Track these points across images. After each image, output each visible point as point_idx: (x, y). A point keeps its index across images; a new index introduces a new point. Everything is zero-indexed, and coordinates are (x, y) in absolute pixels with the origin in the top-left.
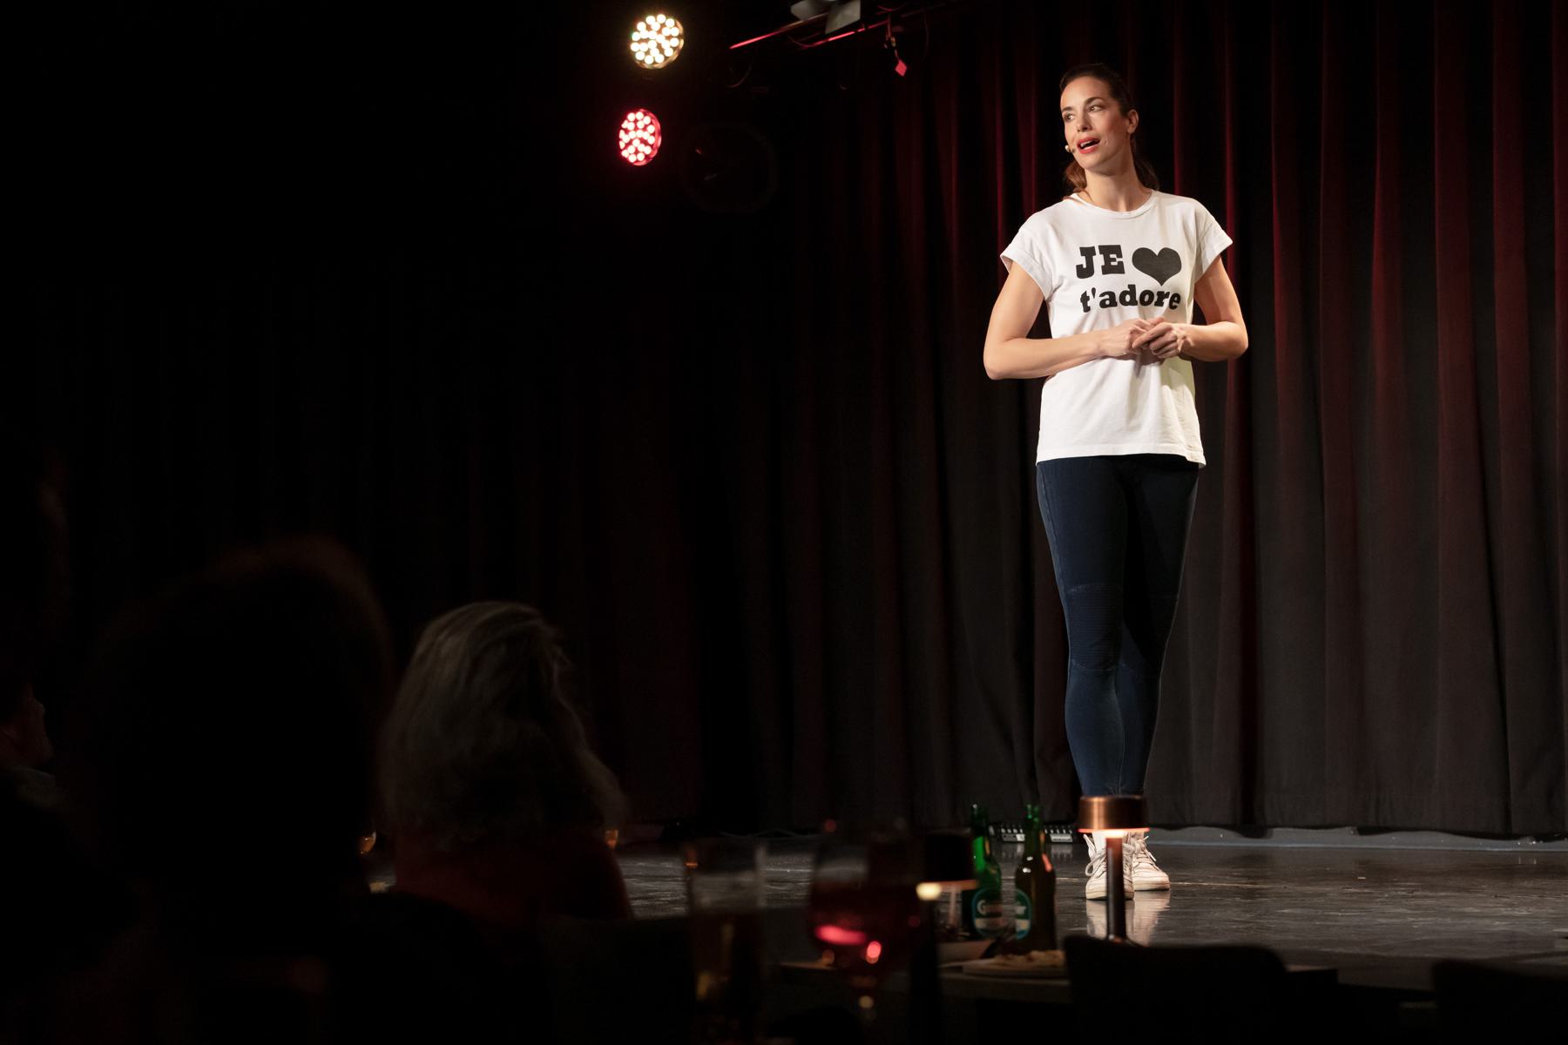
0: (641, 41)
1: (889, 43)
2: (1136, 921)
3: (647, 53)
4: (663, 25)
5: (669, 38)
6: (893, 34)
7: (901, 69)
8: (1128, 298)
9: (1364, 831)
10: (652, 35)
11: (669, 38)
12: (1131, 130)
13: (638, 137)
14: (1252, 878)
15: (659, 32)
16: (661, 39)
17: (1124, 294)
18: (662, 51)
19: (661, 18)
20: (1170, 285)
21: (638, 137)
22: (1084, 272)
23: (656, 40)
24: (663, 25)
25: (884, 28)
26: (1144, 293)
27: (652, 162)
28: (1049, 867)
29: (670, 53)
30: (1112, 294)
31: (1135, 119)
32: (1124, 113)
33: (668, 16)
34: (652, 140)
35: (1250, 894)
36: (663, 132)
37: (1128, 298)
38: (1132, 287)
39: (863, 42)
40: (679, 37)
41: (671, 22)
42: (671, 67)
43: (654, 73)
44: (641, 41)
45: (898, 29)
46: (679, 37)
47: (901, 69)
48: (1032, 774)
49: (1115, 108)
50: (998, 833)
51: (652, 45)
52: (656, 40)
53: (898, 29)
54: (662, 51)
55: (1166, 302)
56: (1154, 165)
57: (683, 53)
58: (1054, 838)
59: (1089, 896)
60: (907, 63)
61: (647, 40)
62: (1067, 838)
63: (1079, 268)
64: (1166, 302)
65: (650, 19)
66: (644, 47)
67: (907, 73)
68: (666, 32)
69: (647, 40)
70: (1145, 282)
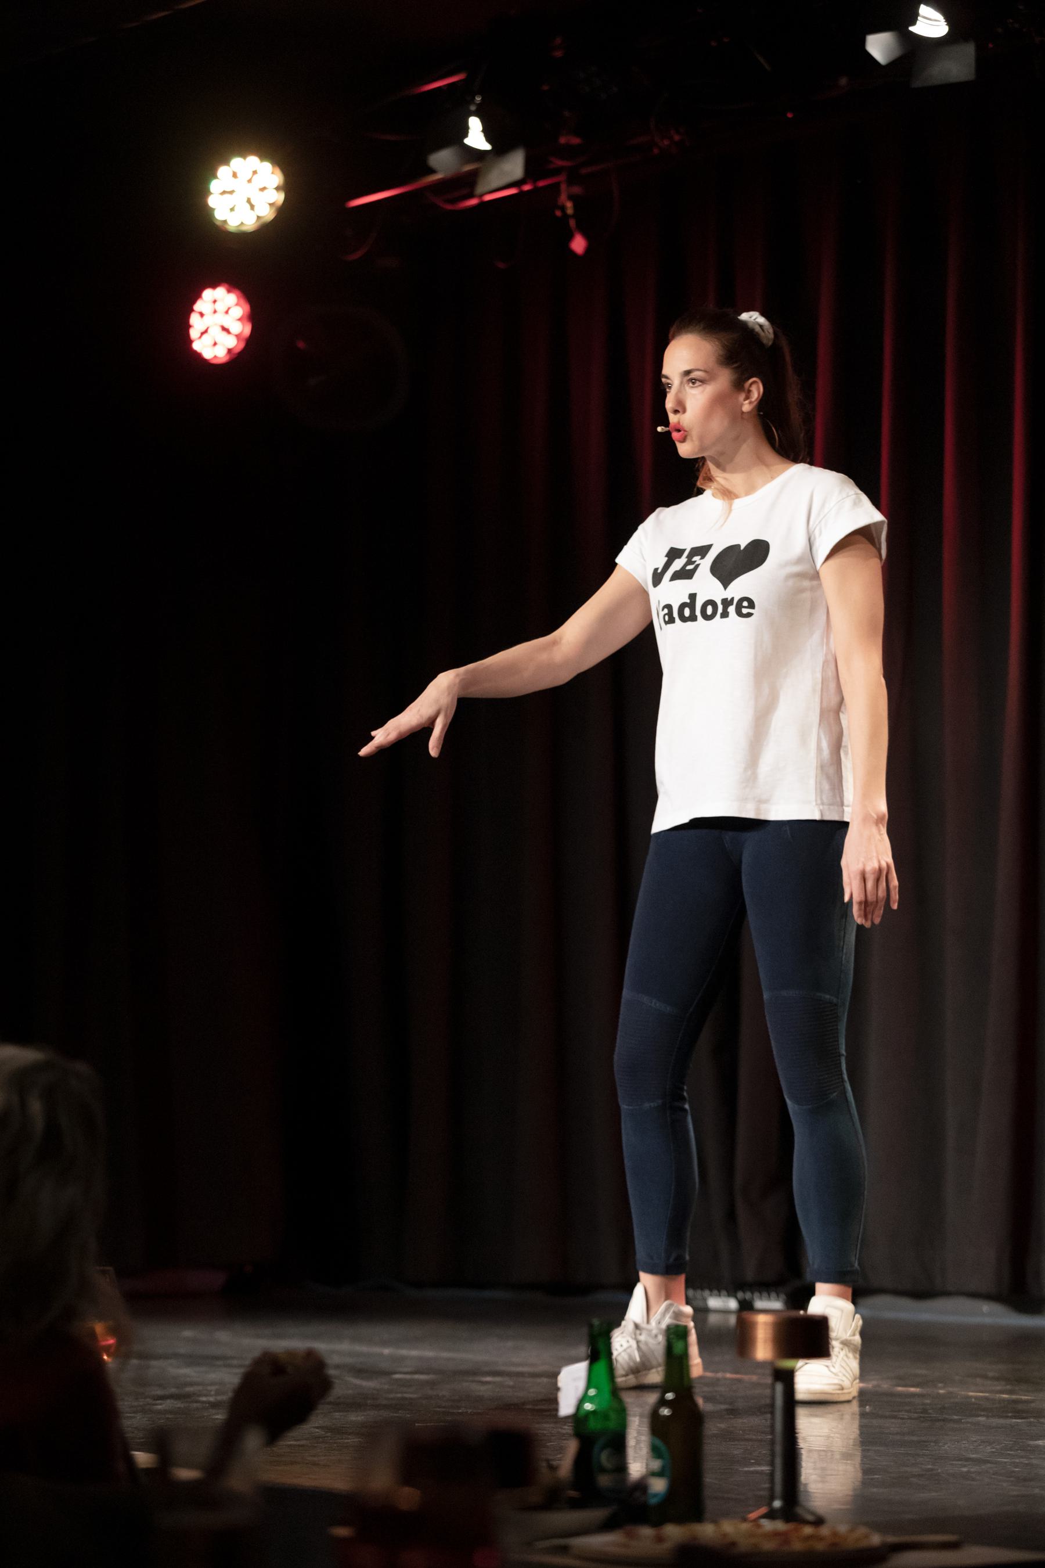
1: (563, 208)
6: (571, 198)
7: (579, 245)
8: (687, 612)
12: (747, 407)
13: (218, 324)
14: (1018, 1380)
17: (682, 607)
20: (742, 586)
21: (218, 324)
22: (657, 578)
23: (245, 192)
25: (556, 187)
27: (237, 360)
29: (237, 328)
30: (669, 607)
31: (757, 390)
32: (739, 385)
35: (1016, 1410)
36: (254, 317)
37: (687, 612)
38: (693, 597)
39: (521, 210)
42: (265, 230)
43: (242, 238)
45: (576, 190)
47: (579, 245)
48: (731, 1216)
49: (724, 378)
51: (216, 333)
52: (245, 192)
53: (576, 190)
55: (732, 609)
56: (788, 435)
57: (283, 212)
60: (586, 236)
62: (733, 1304)
63: (656, 570)
64: (732, 609)
65: (198, 306)
67: (588, 250)
70: (706, 586)
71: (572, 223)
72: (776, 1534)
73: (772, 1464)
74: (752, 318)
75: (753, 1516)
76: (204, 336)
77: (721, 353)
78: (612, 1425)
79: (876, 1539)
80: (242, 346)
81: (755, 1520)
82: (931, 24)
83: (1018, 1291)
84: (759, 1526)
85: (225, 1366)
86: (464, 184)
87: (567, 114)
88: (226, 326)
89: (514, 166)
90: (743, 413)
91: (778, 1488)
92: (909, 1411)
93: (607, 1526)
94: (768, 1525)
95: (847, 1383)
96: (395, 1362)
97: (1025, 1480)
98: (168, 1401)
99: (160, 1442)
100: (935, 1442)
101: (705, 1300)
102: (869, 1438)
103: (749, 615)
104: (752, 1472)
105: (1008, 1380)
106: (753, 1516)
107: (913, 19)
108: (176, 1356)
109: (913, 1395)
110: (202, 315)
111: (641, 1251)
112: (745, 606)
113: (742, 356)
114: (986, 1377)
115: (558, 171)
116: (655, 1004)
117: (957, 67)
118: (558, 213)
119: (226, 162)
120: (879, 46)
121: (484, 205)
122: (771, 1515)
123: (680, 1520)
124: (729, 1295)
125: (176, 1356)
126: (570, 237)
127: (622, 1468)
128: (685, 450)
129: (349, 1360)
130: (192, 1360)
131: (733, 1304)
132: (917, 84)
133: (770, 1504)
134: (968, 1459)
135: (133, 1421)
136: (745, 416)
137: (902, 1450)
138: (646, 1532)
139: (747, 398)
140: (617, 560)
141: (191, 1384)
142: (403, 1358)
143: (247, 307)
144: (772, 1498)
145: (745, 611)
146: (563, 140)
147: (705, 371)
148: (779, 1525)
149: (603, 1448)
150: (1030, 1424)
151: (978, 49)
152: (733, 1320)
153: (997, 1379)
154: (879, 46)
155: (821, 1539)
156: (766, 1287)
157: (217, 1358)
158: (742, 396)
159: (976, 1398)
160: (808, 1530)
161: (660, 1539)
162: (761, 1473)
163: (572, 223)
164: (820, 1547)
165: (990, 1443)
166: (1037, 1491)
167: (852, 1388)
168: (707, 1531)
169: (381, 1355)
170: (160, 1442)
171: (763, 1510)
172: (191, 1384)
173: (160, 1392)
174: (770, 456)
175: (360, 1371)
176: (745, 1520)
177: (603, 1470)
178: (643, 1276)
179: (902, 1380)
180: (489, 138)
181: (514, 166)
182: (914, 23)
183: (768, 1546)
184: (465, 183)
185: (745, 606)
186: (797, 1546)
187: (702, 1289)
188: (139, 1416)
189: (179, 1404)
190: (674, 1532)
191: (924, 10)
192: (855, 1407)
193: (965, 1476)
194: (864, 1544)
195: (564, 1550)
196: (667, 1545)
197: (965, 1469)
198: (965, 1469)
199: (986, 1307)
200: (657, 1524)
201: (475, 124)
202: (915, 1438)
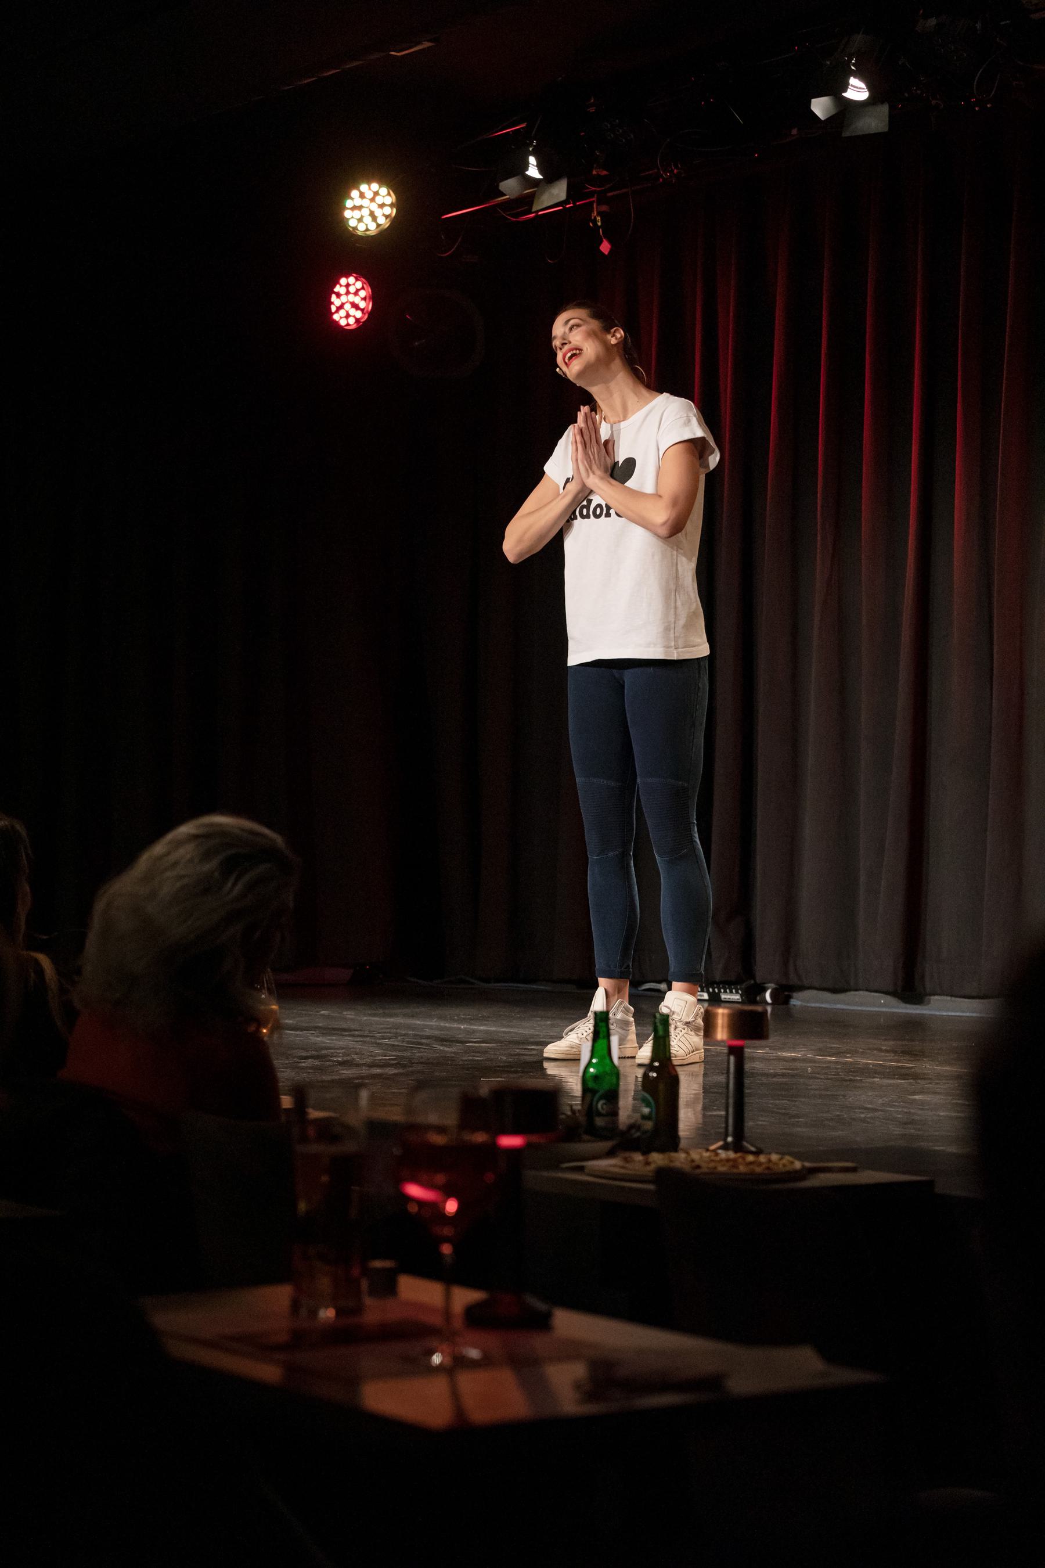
0: (354, 208)
1: (595, 221)
3: (360, 220)
4: (376, 194)
7: (605, 247)
13: (350, 302)
14: (908, 1053)
15: (372, 200)
18: (374, 218)
19: (375, 186)
21: (350, 302)
23: (369, 207)
24: (376, 194)
33: (381, 183)
34: (362, 305)
40: (392, 205)
41: (384, 191)
42: (383, 235)
44: (354, 208)
45: (604, 208)
46: (392, 205)
47: (605, 247)
51: (365, 212)
52: (369, 207)
53: (604, 208)
54: (374, 218)
60: (610, 242)
61: (360, 208)
66: (357, 214)
68: (379, 200)
72: (728, 1160)
73: (727, 1111)
75: (712, 1147)
79: (798, 1165)
81: (714, 1151)
82: (857, 91)
83: (909, 989)
84: (717, 1154)
85: (350, 1036)
86: (525, 202)
89: (559, 191)
91: (731, 1129)
92: (826, 1074)
93: (610, 1154)
94: (723, 1154)
96: (471, 1031)
97: (906, 1123)
98: (310, 1060)
99: (300, 1093)
100: (844, 1096)
104: (715, 1116)
105: (895, 1052)
106: (712, 1147)
107: (845, 87)
108: (316, 1028)
109: (830, 1062)
110: (362, 196)
111: (599, 963)
114: (881, 1050)
115: (591, 194)
117: (875, 122)
120: (820, 107)
121: (538, 217)
122: (726, 1147)
123: (661, 1150)
124: (702, 991)
125: (316, 1028)
127: (614, 1113)
129: (437, 1033)
130: (327, 1031)
132: (846, 134)
133: (725, 1140)
134: (866, 1108)
135: (285, 1075)
137: (820, 1101)
138: (638, 1157)
140: (546, 468)
141: (326, 1048)
142: (474, 1031)
144: (727, 1136)
148: (731, 1155)
149: (600, 1098)
150: (910, 1084)
151: (890, 108)
153: (886, 1051)
154: (820, 107)
155: (760, 1164)
156: (729, 984)
157: (344, 1030)
159: (873, 1065)
160: (751, 1158)
161: (648, 1163)
162: (721, 1116)
164: (758, 1170)
165: (881, 1097)
166: (913, 1131)
168: (679, 1159)
169: (460, 1029)
170: (300, 1093)
171: (721, 1143)
172: (326, 1048)
173: (304, 1054)
174: (644, 392)
175: (443, 1040)
176: (707, 1150)
177: (599, 1114)
178: (602, 981)
179: (822, 1052)
180: (541, 173)
181: (559, 191)
182: (845, 91)
183: (722, 1169)
184: (525, 202)
186: (742, 1169)
188: (288, 1070)
189: (317, 1063)
190: (658, 1159)
191: (853, 81)
193: (864, 1120)
194: (789, 1168)
195: (581, 1169)
196: (653, 1167)
197: (863, 1116)
198: (863, 1116)
199: (883, 999)
200: (646, 1152)
201: (532, 160)
202: (828, 1093)
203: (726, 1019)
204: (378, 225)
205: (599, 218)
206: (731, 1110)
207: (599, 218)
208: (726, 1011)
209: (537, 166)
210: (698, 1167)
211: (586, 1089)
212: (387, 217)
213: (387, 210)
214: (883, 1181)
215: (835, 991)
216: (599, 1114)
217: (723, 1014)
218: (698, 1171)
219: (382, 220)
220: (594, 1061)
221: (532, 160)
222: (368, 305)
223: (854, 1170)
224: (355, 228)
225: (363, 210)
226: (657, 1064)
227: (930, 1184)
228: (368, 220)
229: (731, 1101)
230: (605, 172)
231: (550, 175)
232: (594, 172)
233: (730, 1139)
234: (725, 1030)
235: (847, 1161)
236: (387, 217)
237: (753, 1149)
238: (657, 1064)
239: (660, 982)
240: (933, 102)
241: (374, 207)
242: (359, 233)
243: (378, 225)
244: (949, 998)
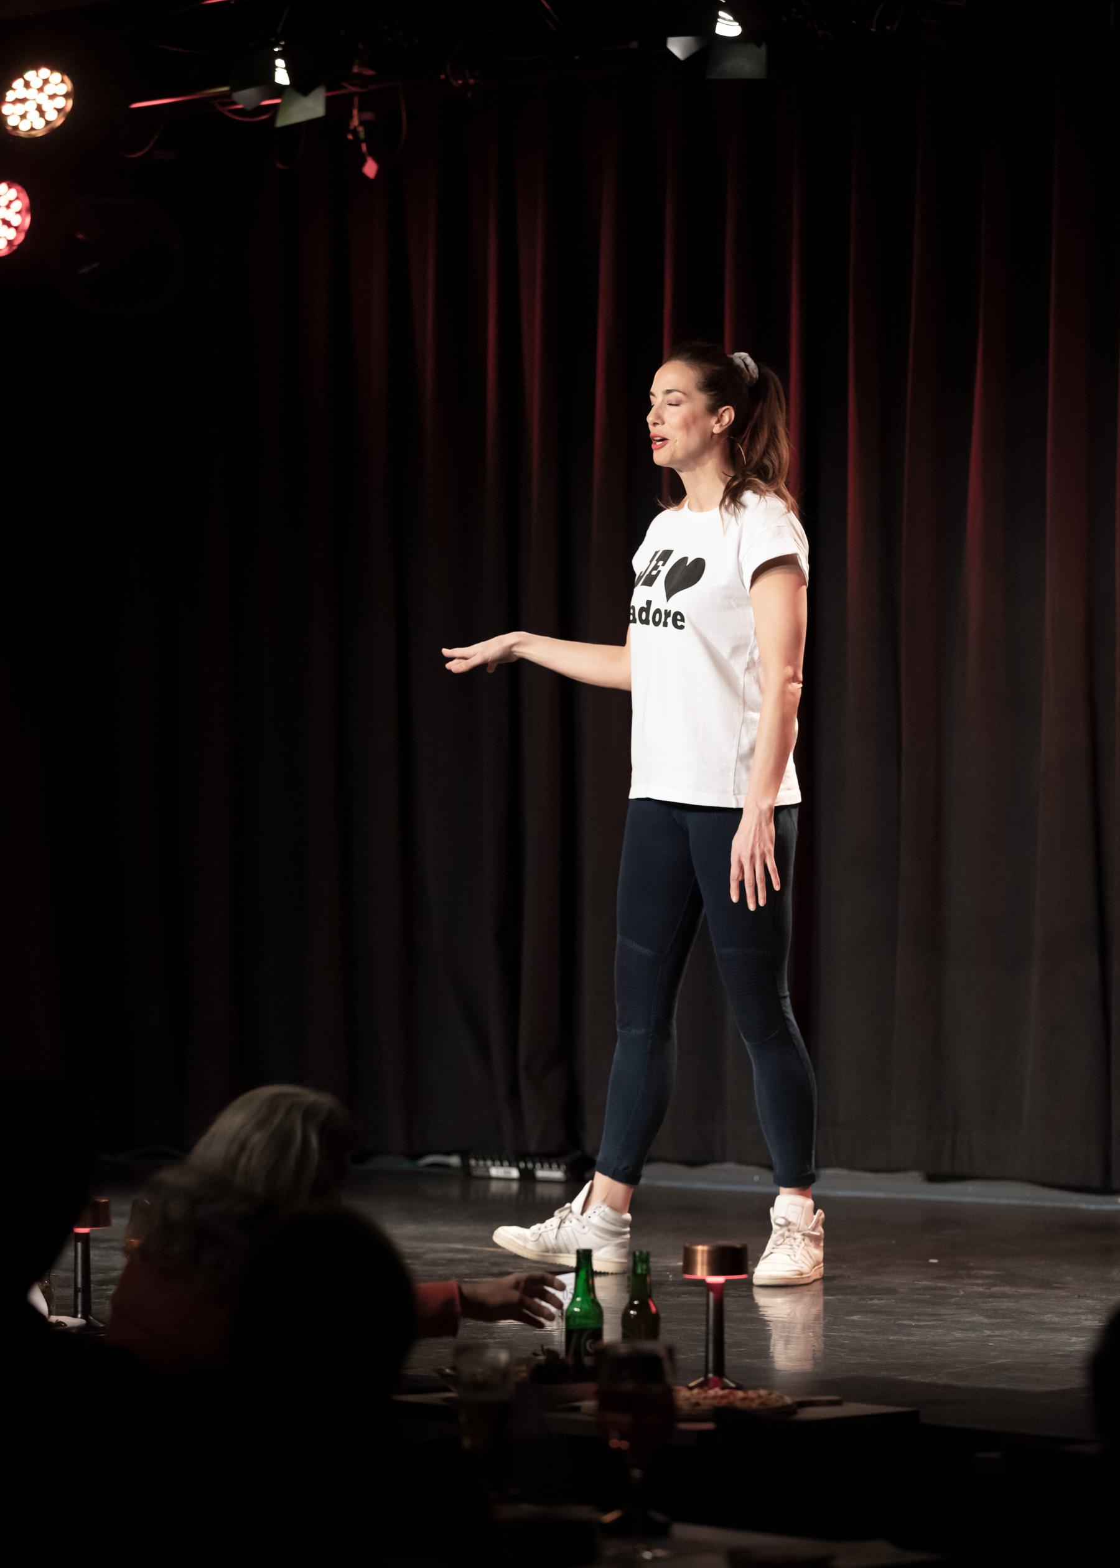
0: (17, 101)
2: (791, 1364)
3: (23, 117)
4: (46, 81)
5: (52, 97)
7: (370, 169)
9: (934, 1177)
10: (31, 93)
11: (52, 97)
12: (717, 429)
15: (41, 90)
16: (42, 99)
18: (41, 112)
19: (45, 72)
20: (682, 601)
24: (46, 81)
26: (658, 611)
28: (653, 1309)
31: (728, 415)
33: (53, 68)
34: (16, 220)
36: (34, 209)
38: (649, 603)
40: (66, 96)
41: (56, 77)
42: (54, 135)
44: (17, 101)
45: (369, 116)
46: (66, 96)
47: (370, 169)
48: (514, 1091)
49: (701, 400)
50: (465, 1165)
51: (30, 107)
54: (41, 112)
55: (670, 620)
58: (541, 1174)
59: (756, 1281)
60: (377, 160)
61: (23, 101)
62: (514, 1173)
65: (30, 75)
66: (20, 109)
67: (379, 173)
68: (49, 89)
69: (23, 101)
71: (364, 147)
74: (743, 358)
76: (19, 105)
77: (702, 380)
78: (591, 1323)
80: (22, 237)
87: (361, 46)
88: (44, 108)
90: (713, 434)
91: (711, 1365)
95: (806, 1268)
101: (487, 1169)
102: (831, 1316)
103: (682, 627)
110: (27, 85)
112: (677, 619)
113: (720, 387)
116: (646, 951)
117: (747, 66)
118: (350, 137)
119: (20, 75)
124: (510, 1166)
126: (363, 162)
128: (660, 457)
131: (514, 1173)
132: (712, 76)
136: (715, 437)
139: (718, 421)
143: (27, 200)
144: (707, 1372)
145: (679, 623)
146: (356, 70)
147: (684, 393)
149: (587, 1339)
152: (515, 1186)
156: (548, 1158)
158: (714, 420)
163: (364, 147)
166: (869, 1360)
167: (819, 1272)
177: (588, 1354)
185: (677, 619)
187: (485, 1159)
191: (721, 13)
192: (819, 1286)
201: (280, 63)
203: (705, 1255)
204: (48, 123)
205: (361, 129)
206: (711, 1346)
207: (361, 129)
208: (705, 1248)
209: (286, 68)
210: (698, 1404)
211: (569, 1333)
212: (59, 111)
213: (61, 103)
214: (827, 1416)
215: (692, 1163)
216: (588, 1354)
217: (703, 1251)
218: (699, 1408)
219: (52, 115)
220: (578, 1299)
221: (280, 63)
222: (23, 220)
223: (837, 1403)
224: (16, 128)
225: (27, 103)
226: (636, 1303)
227: (914, 1415)
228: (33, 115)
229: (711, 1337)
230: (371, 73)
231: (301, 84)
232: (356, 70)
233: (710, 1375)
234: (705, 1267)
235: (832, 1394)
236: (59, 111)
237: (733, 1385)
238: (636, 1303)
239: (449, 1153)
240: (820, 33)
241: (42, 99)
242: (22, 135)
243: (48, 123)
244: (843, 1172)
